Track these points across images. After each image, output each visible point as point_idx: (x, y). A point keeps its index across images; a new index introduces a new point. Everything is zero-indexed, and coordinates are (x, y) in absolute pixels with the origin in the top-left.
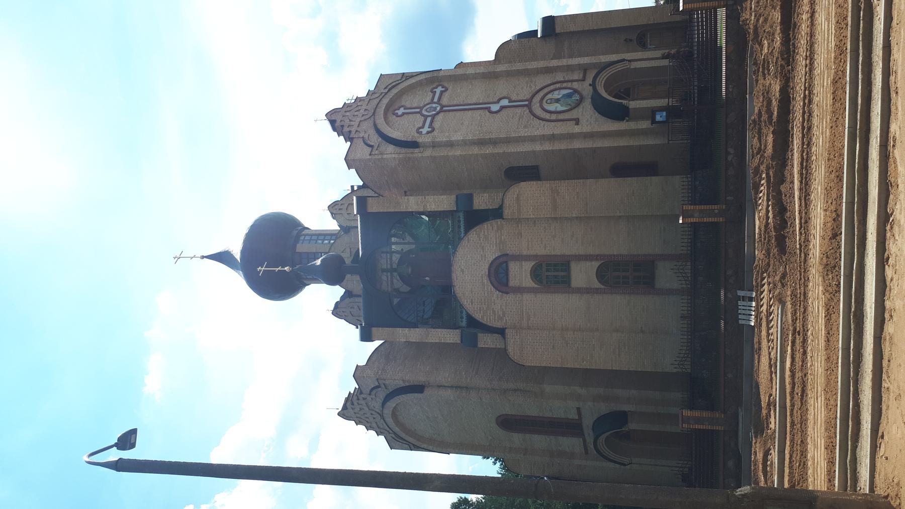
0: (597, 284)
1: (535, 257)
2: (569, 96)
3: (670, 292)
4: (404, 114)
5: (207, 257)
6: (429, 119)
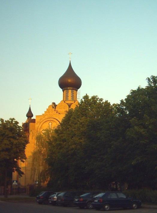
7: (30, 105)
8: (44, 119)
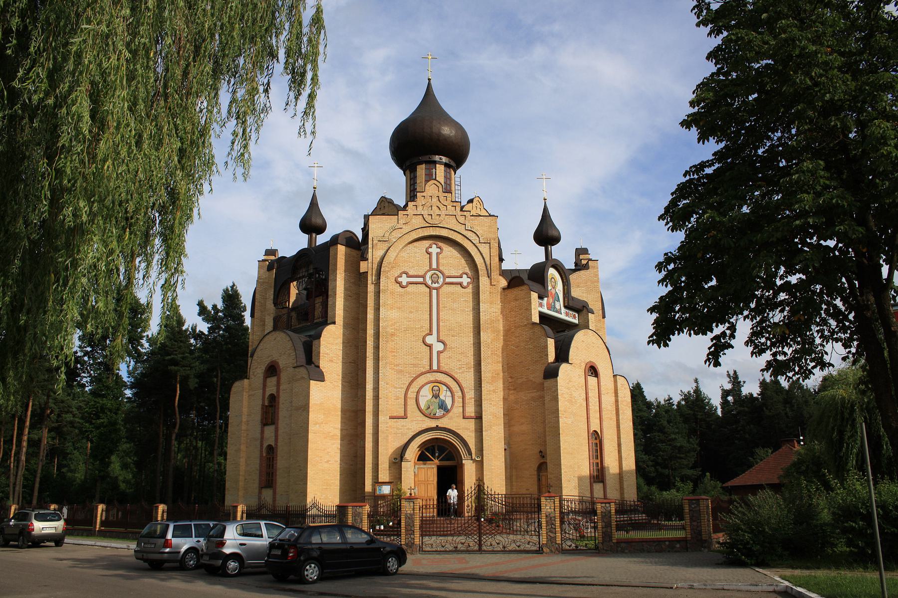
0: (265, 445)
1: (278, 395)
2: (442, 406)
3: (260, 498)
4: (430, 254)
5: (429, 85)
6: (421, 280)
7: (429, 80)
8: (406, 229)
